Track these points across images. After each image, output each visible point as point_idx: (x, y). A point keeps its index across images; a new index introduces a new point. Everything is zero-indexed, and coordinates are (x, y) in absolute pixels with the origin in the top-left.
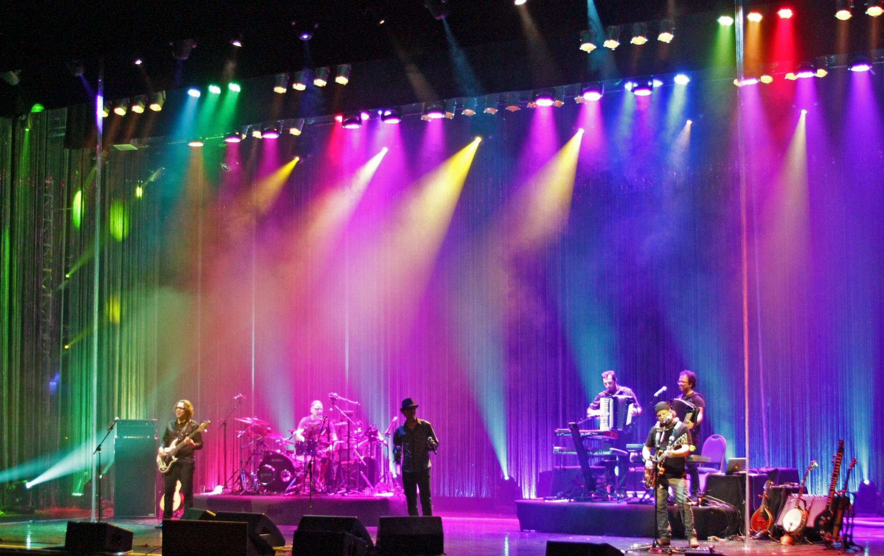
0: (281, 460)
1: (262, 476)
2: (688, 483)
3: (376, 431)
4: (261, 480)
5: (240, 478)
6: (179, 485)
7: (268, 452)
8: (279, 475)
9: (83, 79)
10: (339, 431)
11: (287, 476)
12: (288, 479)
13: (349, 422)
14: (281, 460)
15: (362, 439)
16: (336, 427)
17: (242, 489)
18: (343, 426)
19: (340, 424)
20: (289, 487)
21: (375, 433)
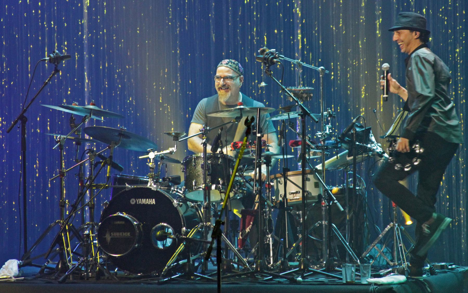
0: (123, 223)
1: (108, 237)
2: (431, 61)
3: (367, 132)
4: (105, 247)
5: (59, 241)
6: (305, 43)
7: (122, 181)
8: (147, 239)
9: (462, 205)
10: (284, 132)
11: (163, 237)
12: (169, 242)
13: (304, 114)
14: (123, 223)
15: (336, 148)
16: (275, 123)
17: (65, 268)
18: (292, 122)
19: (285, 117)
20: (171, 262)
21: (364, 137)
